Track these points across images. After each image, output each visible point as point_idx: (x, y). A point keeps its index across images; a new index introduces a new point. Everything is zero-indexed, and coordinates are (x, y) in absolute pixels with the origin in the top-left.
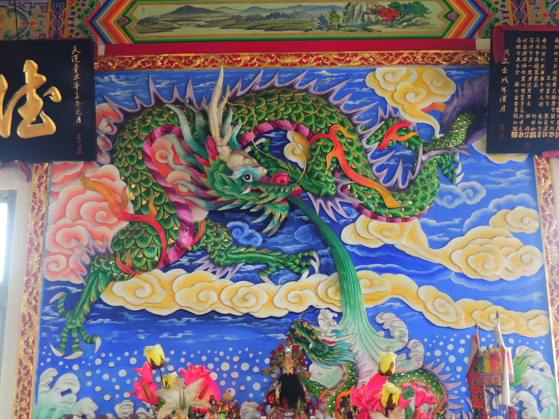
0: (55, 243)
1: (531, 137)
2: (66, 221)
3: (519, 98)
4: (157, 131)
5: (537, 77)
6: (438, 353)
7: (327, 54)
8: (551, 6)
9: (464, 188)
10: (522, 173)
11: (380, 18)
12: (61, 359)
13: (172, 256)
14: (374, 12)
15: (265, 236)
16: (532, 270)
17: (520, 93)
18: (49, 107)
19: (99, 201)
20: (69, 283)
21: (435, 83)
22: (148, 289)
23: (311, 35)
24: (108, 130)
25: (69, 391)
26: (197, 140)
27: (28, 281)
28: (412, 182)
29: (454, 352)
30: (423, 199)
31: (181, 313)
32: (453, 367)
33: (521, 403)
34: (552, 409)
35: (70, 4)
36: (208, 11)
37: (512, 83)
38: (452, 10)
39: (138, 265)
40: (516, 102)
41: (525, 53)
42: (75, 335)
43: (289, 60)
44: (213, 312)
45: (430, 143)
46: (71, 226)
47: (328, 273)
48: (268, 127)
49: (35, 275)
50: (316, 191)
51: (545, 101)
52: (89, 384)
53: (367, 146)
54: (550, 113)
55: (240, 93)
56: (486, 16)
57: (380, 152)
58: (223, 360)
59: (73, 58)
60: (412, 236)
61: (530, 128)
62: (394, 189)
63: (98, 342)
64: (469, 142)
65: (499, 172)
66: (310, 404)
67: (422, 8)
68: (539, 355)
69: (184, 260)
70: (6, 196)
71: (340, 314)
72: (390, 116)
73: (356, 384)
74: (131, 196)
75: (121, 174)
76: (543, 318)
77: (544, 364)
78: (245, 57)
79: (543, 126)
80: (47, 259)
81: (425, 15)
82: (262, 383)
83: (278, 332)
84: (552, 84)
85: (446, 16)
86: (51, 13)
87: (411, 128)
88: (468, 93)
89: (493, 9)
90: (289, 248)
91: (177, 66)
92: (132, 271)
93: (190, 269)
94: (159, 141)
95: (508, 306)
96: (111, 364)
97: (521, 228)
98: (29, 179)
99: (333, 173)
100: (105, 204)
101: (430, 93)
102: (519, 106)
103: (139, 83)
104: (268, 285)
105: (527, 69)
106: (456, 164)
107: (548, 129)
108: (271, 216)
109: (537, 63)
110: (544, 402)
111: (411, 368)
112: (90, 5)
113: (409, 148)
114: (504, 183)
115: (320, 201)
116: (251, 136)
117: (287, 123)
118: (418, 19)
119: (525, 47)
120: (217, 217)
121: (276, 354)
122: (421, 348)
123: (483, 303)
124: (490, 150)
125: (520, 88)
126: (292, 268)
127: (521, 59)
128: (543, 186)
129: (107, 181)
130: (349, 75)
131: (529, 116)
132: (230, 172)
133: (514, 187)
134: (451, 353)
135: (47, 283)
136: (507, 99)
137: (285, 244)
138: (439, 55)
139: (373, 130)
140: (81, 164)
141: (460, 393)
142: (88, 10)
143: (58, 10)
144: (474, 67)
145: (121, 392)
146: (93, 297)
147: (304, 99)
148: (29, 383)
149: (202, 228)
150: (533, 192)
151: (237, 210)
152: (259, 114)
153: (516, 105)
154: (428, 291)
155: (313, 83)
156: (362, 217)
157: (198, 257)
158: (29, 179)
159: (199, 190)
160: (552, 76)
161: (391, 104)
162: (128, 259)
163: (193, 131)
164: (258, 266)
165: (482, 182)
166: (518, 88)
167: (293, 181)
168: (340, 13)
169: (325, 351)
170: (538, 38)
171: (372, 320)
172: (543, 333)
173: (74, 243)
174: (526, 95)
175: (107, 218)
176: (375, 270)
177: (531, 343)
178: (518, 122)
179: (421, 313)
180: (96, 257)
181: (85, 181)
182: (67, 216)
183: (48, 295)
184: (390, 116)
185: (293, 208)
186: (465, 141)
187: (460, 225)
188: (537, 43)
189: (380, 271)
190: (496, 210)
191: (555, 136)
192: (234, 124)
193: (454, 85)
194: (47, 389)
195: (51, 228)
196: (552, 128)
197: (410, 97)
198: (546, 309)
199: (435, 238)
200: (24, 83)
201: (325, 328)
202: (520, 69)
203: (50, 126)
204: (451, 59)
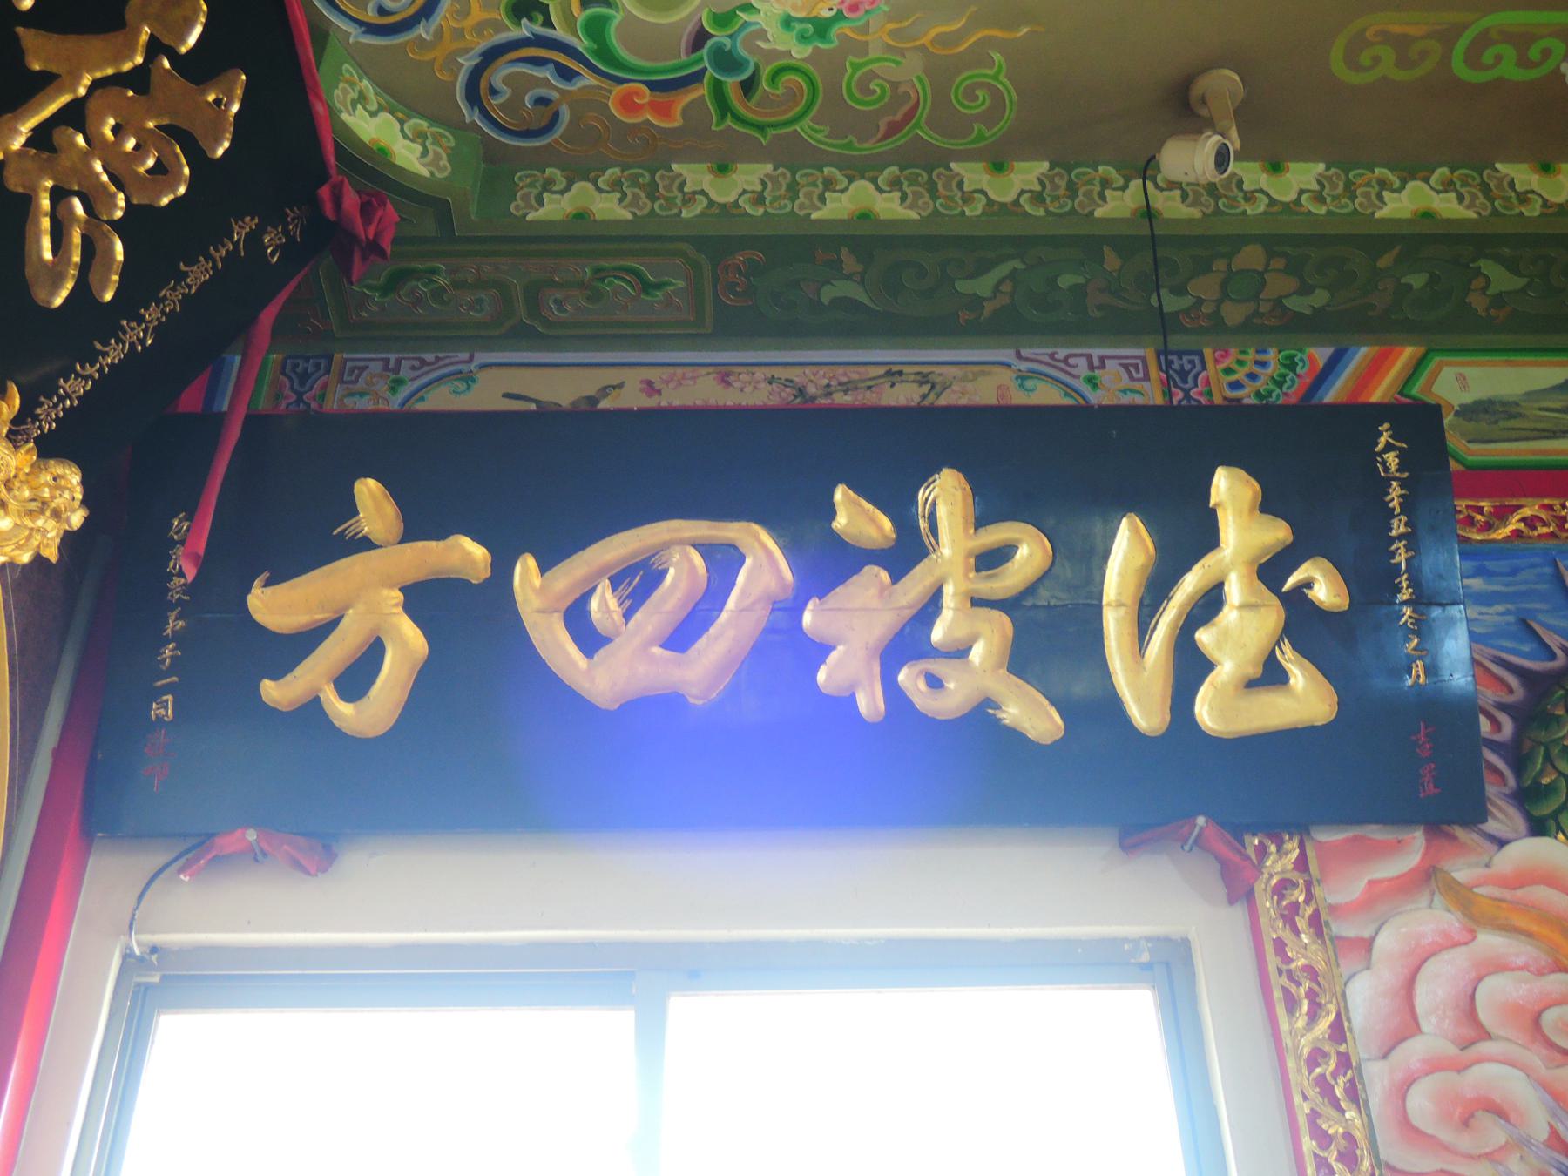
0: (1409, 1130)
18: (1303, 623)
35: (1217, 361)
59: (1384, 463)
70: (1145, 958)
103: (1526, 582)
112: (1285, 366)
142: (1284, 376)
173: (1495, 1134)
181: (1461, 897)
182: (1425, 1026)
203: (1306, 697)
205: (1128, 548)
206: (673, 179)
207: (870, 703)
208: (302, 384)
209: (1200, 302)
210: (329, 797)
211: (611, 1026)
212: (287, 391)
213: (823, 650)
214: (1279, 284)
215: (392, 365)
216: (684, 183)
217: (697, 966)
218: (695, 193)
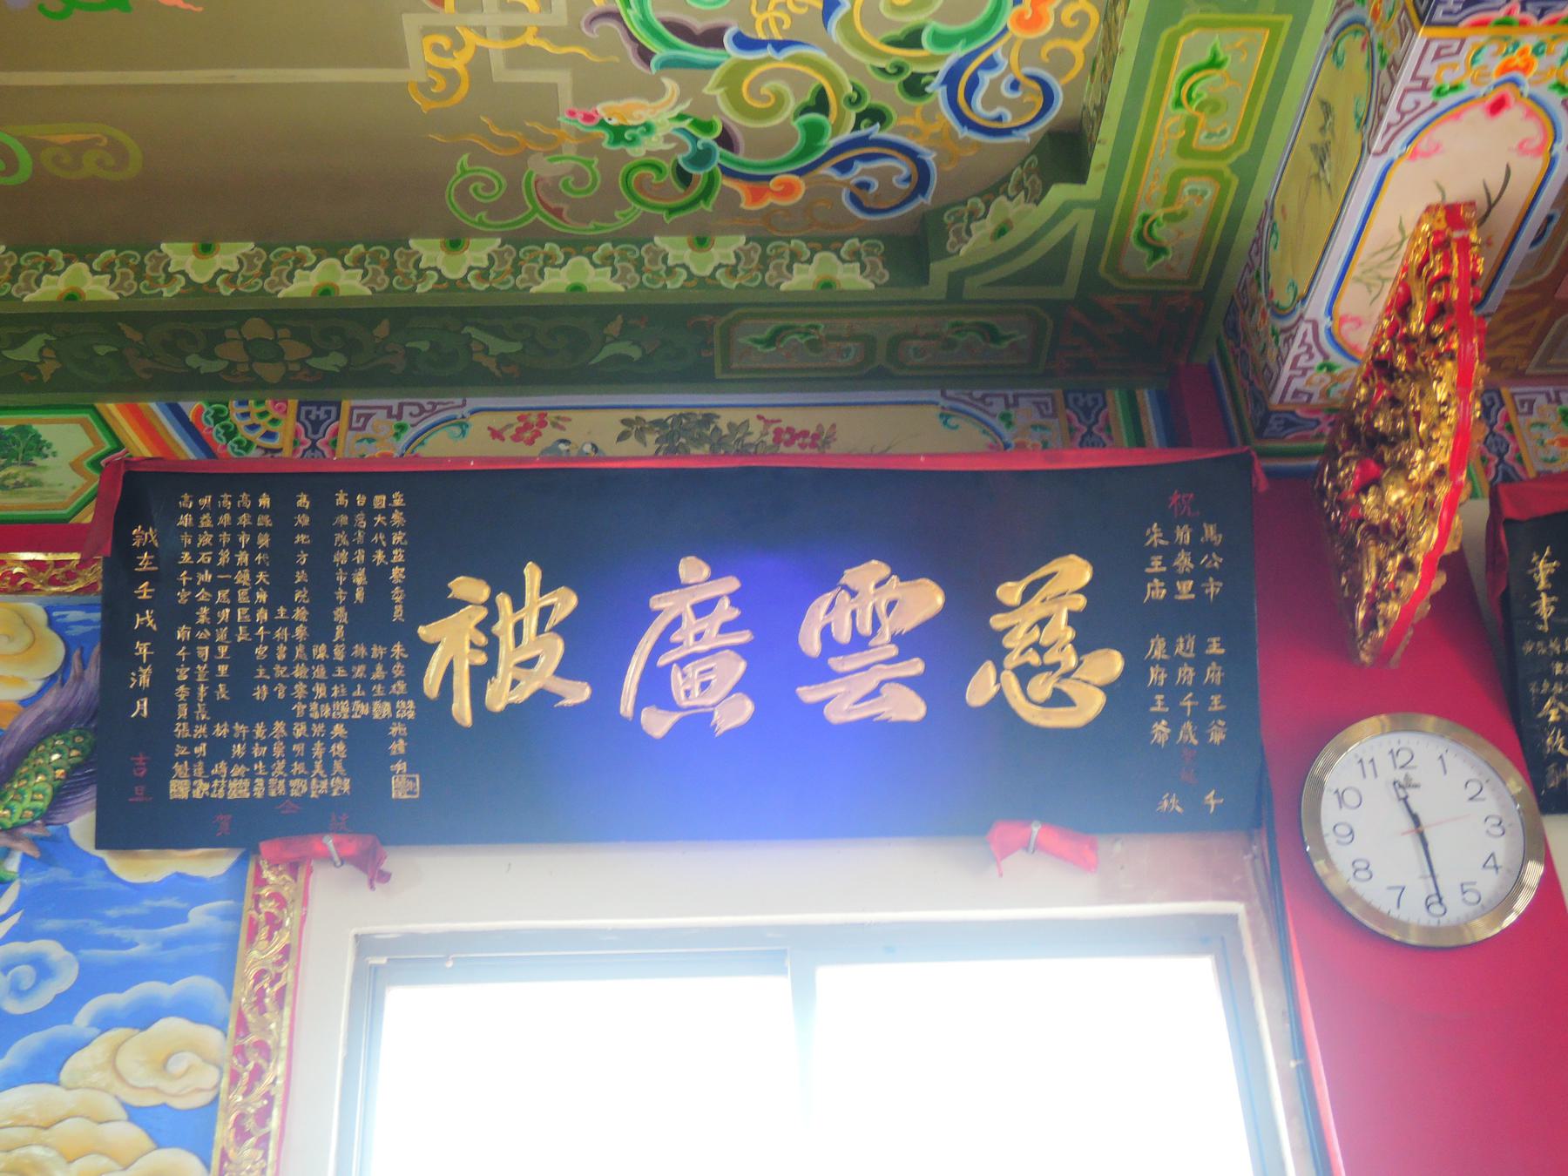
1: (232, 795)
3: (192, 675)
5: (246, 610)
10: (209, 913)
17: (193, 661)
37: (167, 628)
40: (182, 688)
41: (206, 539)
51: (272, 683)
54: (290, 720)
61: (230, 767)
64: (59, 818)
65: (133, 911)
67: (32, 443)
79: (269, 760)
81: (37, 461)
84: (292, 631)
86: (297, 433)
89: (239, 443)
97: (156, 1089)
102: (192, 701)
105: (213, 587)
107: (288, 768)
109: (242, 567)
114: (143, 945)
118: (12, 470)
119: (206, 521)
124: (105, 838)
125: (192, 644)
127: (195, 556)
131: (225, 731)
133: (171, 955)
136: (152, 678)
150: (225, 971)
153: (182, 697)
160: (292, 606)
165: (71, 941)
166: (186, 643)
170: (226, 496)
174: (213, 663)
178: (191, 749)
188: (243, 510)
190: (95, 1031)
191: (309, 792)
193: (59, 650)
196: (298, 767)
206: (409, 256)
208: (315, 432)
209: (232, 365)
211: (776, 987)
212: (303, 437)
214: (295, 350)
215: (395, 411)
216: (419, 260)
218: (603, 265)
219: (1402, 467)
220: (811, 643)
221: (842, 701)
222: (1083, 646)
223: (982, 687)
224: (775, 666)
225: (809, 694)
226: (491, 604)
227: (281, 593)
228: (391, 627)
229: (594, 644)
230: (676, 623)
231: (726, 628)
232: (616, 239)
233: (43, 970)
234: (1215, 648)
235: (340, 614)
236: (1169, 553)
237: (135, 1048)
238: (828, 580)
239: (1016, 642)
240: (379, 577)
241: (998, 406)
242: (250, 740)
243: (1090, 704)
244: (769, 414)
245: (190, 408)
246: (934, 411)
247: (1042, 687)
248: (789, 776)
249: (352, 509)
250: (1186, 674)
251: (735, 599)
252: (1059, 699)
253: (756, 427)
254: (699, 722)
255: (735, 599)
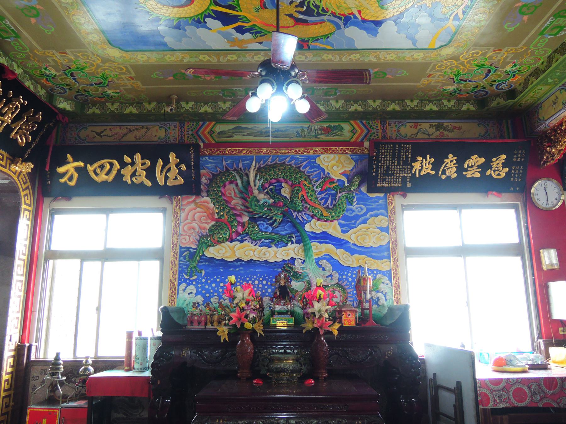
0: (184, 230)
2: (188, 221)
4: (227, 182)
6: (344, 277)
7: (299, 149)
8: (398, 127)
9: (356, 207)
11: (323, 132)
12: (188, 279)
13: (234, 236)
14: (320, 129)
15: (273, 228)
16: (384, 243)
17: (381, 168)
18: (180, 173)
19: (203, 213)
20: (190, 248)
21: (346, 162)
22: (224, 250)
23: (292, 140)
24: (206, 181)
25: (192, 293)
26: (244, 187)
27: (173, 247)
28: (335, 205)
29: (351, 277)
30: (339, 212)
31: (238, 260)
32: (350, 282)
33: (378, 297)
34: (391, 300)
36: (248, 129)
38: (354, 128)
39: (220, 240)
42: (193, 269)
43: (283, 151)
44: (252, 259)
45: (342, 188)
46: (191, 223)
47: (299, 243)
48: (274, 181)
49: (176, 244)
50: (294, 209)
52: (200, 290)
53: (316, 190)
54: (394, 176)
55: (262, 166)
56: (369, 131)
57: (321, 192)
58: (255, 279)
60: (334, 228)
62: (327, 208)
63: (203, 272)
66: (291, 298)
68: (386, 278)
69: (239, 238)
71: (304, 261)
72: (326, 176)
73: (310, 289)
74: (217, 211)
75: (212, 201)
76: (389, 263)
77: (388, 282)
78: (264, 150)
79: (391, 181)
80: (181, 238)
82: (271, 289)
83: (278, 268)
85: (351, 131)
87: (335, 181)
88: (360, 166)
90: (282, 233)
91: (235, 154)
92: (217, 243)
93: (241, 242)
94: (228, 187)
95: (374, 258)
96: (209, 282)
98: (172, 203)
99: (302, 201)
100: (205, 214)
101: (343, 166)
102: (381, 173)
104: (274, 248)
105: (384, 158)
106: (354, 197)
108: (276, 220)
110: (388, 297)
111: (333, 283)
113: (334, 190)
114: (374, 206)
115: (296, 213)
116: (267, 185)
117: (282, 179)
120: (253, 220)
121: (278, 277)
122: (337, 275)
123: (363, 256)
125: (381, 166)
126: (283, 242)
128: (390, 207)
129: (207, 204)
130: (309, 158)
132: (258, 201)
134: (350, 277)
135: (181, 248)
137: (281, 231)
138: (348, 149)
139: (319, 182)
140: (194, 197)
141: (353, 293)
143: (182, 127)
144: (363, 154)
145: (213, 293)
146: (201, 253)
147: (290, 169)
148: (175, 289)
149: (247, 224)
150: (386, 209)
151: (261, 217)
152: (271, 176)
154: (340, 251)
155: (293, 162)
156: (314, 220)
157: (245, 237)
158: (172, 203)
159: (246, 209)
160: (395, 160)
161: (326, 171)
162: (216, 237)
163: (242, 183)
164: (270, 240)
165: (365, 205)
167: (285, 205)
168: (306, 130)
169: (297, 276)
171: (317, 263)
172: (388, 269)
173: (192, 231)
174: (384, 168)
175: (206, 220)
176: (319, 242)
177: (383, 273)
179: (338, 260)
180: (202, 237)
181: (196, 204)
183: (181, 253)
184: (326, 176)
185: (284, 216)
186: (358, 188)
187: (355, 223)
189: (320, 243)
192: (260, 180)
194: (182, 292)
195: (182, 224)
197: (335, 168)
198: (390, 259)
199: (344, 229)
200: (170, 162)
201: (298, 266)
202: (381, 158)
203: (181, 181)
204: (353, 151)
205: (160, 162)
207: (129, 182)
210: (67, 193)
211: (103, 216)
213: (123, 176)
217: (112, 210)
219: (555, 147)
220: (466, 166)
221: (469, 175)
222: (503, 167)
223: (488, 173)
224: (460, 169)
225: (464, 173)
226: (422, 161)
227: (393, 159)
228: (409, 163)
229: (436, 166)
230: (447, 163)
231: (454, 164)
232: (436, 101)
233: (362, 209)
234: (521, 168)
235: (401, 162)
236: (517, 154)
237: (377, 219)
238: (469, 158)
239: (494, 166)
240: (407, 156)
241: (487, 123)
242: (388, 179)
243: (503, 175)
244: (452, 124)
245: (364, 121)
246: (477, 124)
247: (497, 173)
248: (461, 184)
249: (404, 147)
250: (517, 171)
251: (456, 160)
252: (499, 175)
253: (450, 126)
254: (449, 177)
255: (456, 160)
